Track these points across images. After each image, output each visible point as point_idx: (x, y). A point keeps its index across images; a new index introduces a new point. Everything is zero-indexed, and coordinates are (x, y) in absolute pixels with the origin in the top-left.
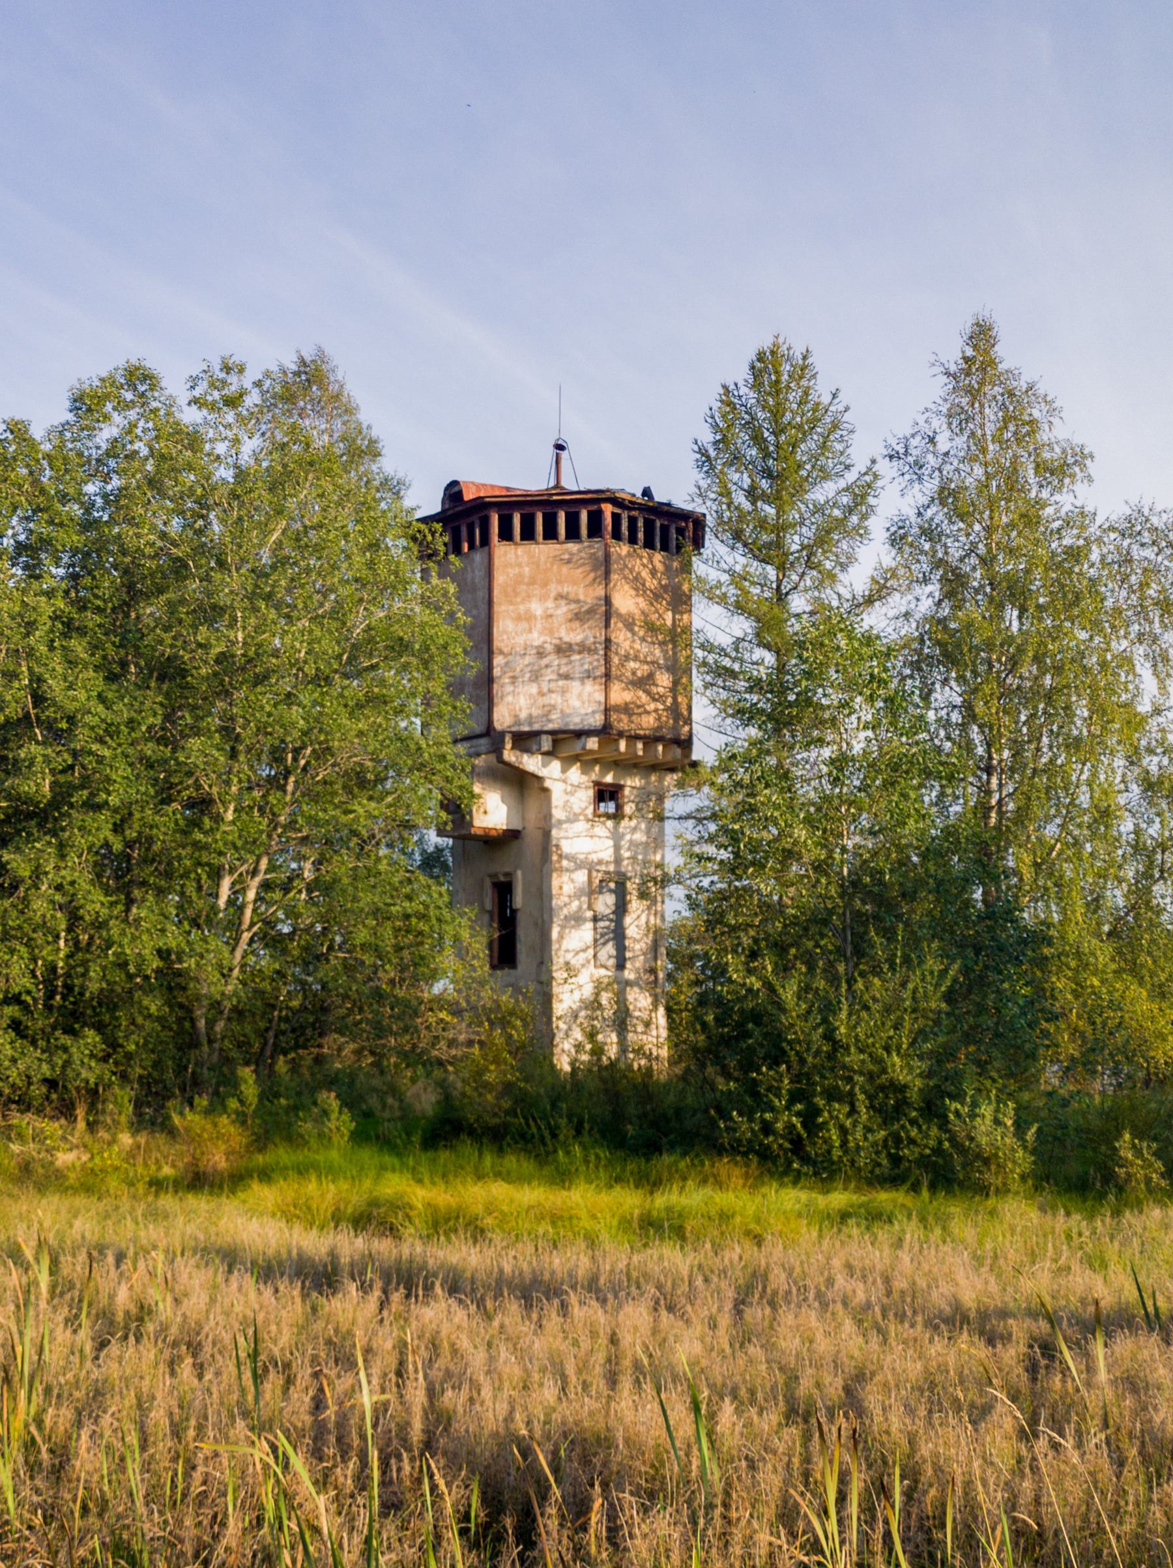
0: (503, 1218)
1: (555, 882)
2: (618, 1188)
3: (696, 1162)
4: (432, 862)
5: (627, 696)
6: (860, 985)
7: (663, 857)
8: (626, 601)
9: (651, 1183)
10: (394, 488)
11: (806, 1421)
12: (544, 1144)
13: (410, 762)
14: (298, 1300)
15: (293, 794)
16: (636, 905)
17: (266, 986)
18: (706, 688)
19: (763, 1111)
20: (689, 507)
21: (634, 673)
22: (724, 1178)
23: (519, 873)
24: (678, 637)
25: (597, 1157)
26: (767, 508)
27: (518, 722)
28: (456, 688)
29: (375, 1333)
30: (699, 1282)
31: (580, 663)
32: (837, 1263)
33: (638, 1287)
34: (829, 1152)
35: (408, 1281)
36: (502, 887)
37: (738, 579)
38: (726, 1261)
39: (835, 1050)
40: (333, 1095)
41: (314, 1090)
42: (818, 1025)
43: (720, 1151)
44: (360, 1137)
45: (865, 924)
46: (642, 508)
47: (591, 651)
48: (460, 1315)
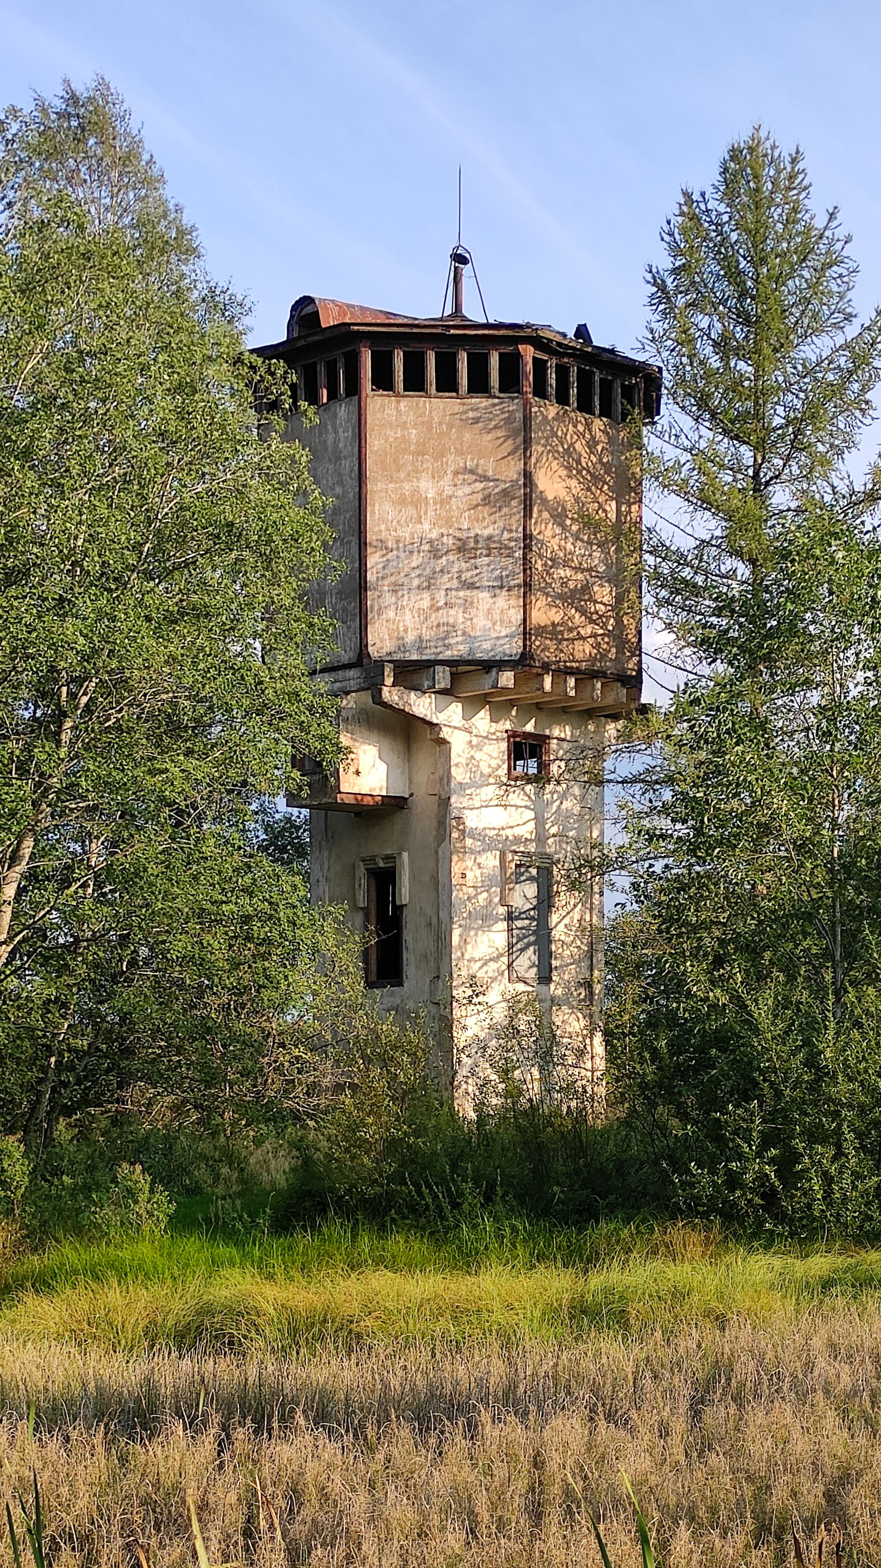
0: (387, 1319)
1: (456, 869)
2: (541, 1267)
3: (642, 1228)
4: (282, 844)
5: (556, 616)
6: (852, 996)
7: (602, 833)
8: (553, 483)
9: (584, 1259)
10: (221, 306)
11: (779, 1539)
12: (443, 1218)
13: (246, 702)
14: (100, 1449)
15: (72, 744)
16: (564, 899)
17: (36, 1019)
18: (660, 606)
19: (729, 1160)
20: (640, 357)
21: (564, 584)
22: (678, 1248)
23: (405, 855)
24: (626, 535)
25: (514, 1229)
26: (742, 365)
27: (402, 647)
28: (311, 599)
29: (212, 1482)
30: (647, 1382)
31: (487, 568)
32: (817, 1343)
33: (569, 1393)
34: (809, 1206)
35: (260, 1412)
36: (380, 877)
37: (704, 459)
38: (681, 1350)
39: (819, 1079)
40: (139, 1168)
41: (113, 1163)
42: (799, 1048)
43: (674, 1213)
44: (182, 1223)
45: (858, 919)
46: (579, 355)
47: (504, 550)
48: (330, 1450)
